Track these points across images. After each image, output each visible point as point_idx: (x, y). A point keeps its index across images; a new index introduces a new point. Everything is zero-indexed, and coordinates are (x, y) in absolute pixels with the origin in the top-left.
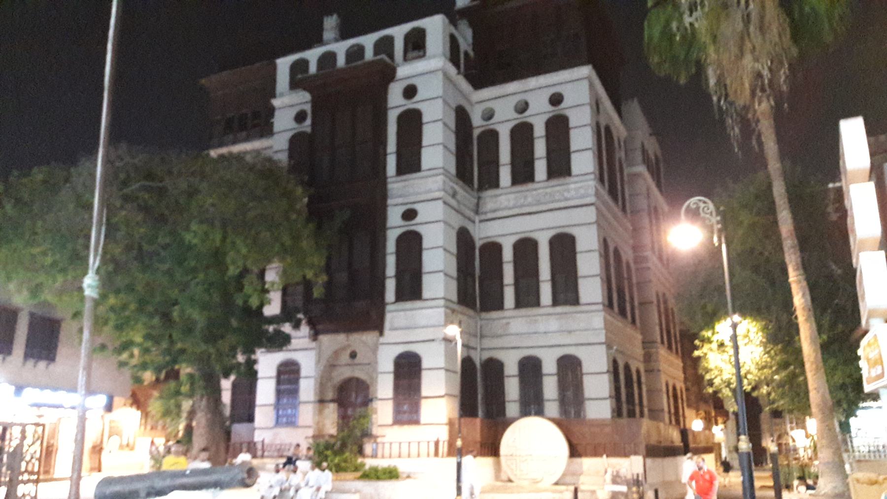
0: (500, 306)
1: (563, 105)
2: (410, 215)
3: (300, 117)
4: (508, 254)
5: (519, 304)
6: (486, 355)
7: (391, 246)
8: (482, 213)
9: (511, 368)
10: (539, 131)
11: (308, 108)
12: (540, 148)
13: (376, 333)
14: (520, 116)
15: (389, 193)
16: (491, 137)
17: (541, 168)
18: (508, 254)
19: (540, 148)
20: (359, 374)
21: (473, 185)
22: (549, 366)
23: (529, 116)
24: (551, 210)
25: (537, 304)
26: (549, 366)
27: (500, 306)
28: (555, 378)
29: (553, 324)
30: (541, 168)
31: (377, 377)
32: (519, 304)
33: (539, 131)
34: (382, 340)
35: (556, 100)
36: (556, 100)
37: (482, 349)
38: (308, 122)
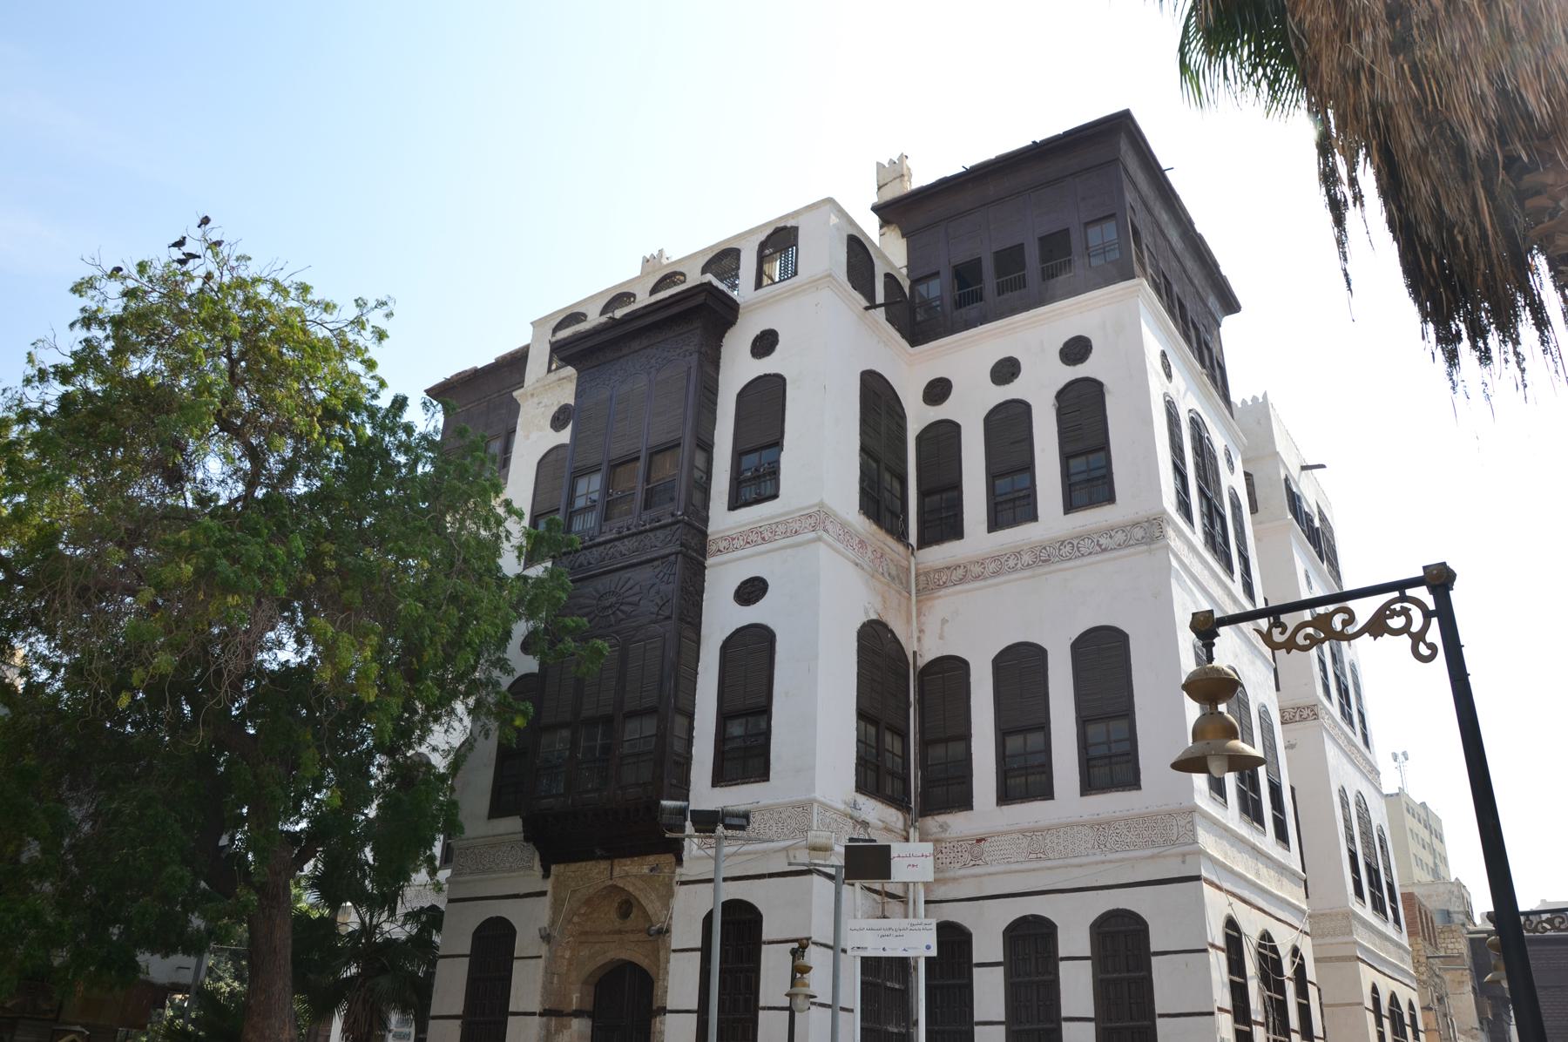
3: (558, 422)
13: (670, 858)
15: (712, 548)
16: (943, 438)
20: (638, 956)
22: (1074, 940)
26: (1074, 940)
31: (668, 961)
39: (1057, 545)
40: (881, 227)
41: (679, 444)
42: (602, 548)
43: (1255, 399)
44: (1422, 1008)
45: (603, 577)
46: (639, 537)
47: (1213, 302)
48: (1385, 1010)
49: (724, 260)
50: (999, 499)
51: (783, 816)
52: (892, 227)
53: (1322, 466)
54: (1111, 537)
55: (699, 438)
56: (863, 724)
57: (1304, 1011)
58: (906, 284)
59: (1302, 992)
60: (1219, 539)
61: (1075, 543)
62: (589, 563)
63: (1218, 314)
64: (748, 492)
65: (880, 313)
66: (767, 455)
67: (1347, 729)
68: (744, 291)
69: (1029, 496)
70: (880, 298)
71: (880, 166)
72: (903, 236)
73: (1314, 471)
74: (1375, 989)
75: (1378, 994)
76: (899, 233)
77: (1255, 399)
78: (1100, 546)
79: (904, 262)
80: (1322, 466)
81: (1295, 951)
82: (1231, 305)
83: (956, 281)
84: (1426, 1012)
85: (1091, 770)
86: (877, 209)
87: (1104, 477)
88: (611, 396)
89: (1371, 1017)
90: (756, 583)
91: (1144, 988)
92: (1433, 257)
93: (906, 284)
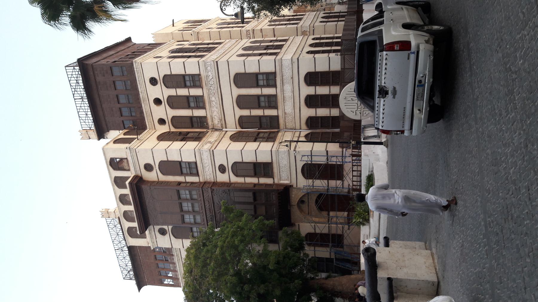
0: (276, 118)
1: (158, 78)
2: (222, 169)
4: (246, 113)
5: (276, 107)
6: (304, 126)
7: (241, 180)
8: (222, 127)
9: (311, 112)
10: (172, 92)
11: (157, 228)
12: (182, 92)
14: (163, 103)
16: (175, 121)
17: (195, 92)
18: (246, 113)
19: (182, 92)
21: (203, 132)
23: (164, 98)
24: (236, 124)
25: (275, 96)
27: (276, 118)
28: (317, 87)
29: (288, 88)
30: (195, 92)
32: (276, 107)
33: (172, 92)
34: (295, 186)
35: (153, 81)
36: (153, 81)
37: (300, 129)
38: (165, 227)
39: (210, 90)
40: (104, 138)
41: (178, 190)
42: (207, 212)
43: (153, 37)
44: (324, 11)
45: (215, 211)
46: (205, 201)
47: (129, 44)
48: (327, 20)
49: (119, 182)
50: (196, 106)
51: (281, 158)
52: (105, 135)
53: (173, 20)
54: (209, 76)
55: (177, 185)
56: (257, 141)
57: (327, 38)
58: (126, 131)
59: (323, 38)
60: (206, 49)
61: (210, 86)
62: (211, 216)
63: (132, 44)
64: (194, 171)
65: (139, 137)
66: (183, 165)
67: (197, 28)
68: (130, 174)
69: (196, 98)
70: (136, 137)
71: (82, 139)
72: (108, 131)
73: (174, 22)
74: (321, 22)
75: (322, 21)
76: (107, 132)
77: (153, 37)
78: (212, 79)
79: (118, 131)
80: (173, 20)
81: (313, 39)
82: (129, 40)
83: (423, 3)
84: (325, 10)
85: (270, 85)
86: (99, 139)
87: (192, 77)
88: (160, 213)
89: (328, 23)
90: (220, 168)
91: (323, 74)
92: (502, 6)
93: (126, 131)
